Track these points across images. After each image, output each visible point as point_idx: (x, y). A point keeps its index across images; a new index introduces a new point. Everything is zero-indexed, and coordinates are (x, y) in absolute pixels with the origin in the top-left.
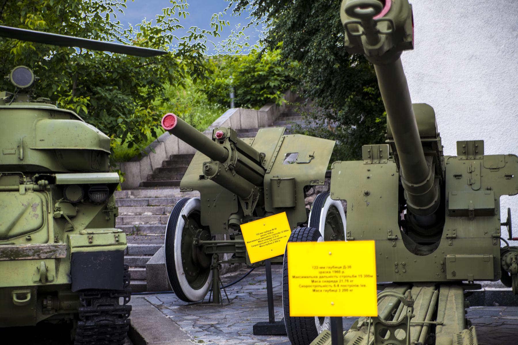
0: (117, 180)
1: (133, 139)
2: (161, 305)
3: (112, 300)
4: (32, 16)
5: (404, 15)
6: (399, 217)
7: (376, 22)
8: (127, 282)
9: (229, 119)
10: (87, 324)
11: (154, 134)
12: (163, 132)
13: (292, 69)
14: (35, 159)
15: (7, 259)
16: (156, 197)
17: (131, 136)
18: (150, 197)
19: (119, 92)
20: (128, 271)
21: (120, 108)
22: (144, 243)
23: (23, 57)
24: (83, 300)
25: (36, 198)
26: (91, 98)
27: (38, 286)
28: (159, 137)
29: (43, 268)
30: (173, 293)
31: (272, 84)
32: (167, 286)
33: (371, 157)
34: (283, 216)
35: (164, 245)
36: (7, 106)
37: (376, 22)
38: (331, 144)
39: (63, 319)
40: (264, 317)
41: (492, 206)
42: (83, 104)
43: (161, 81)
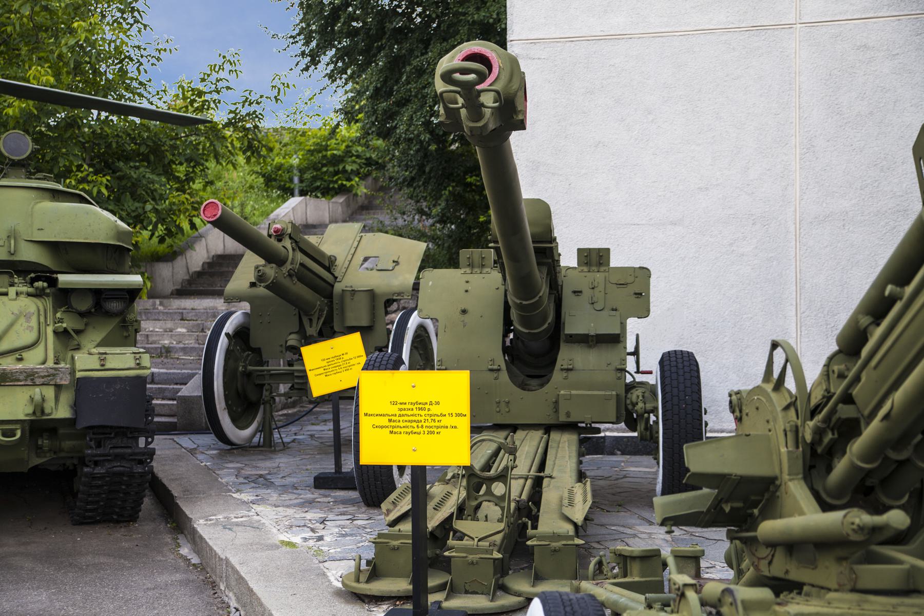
2: (195, 449)
6: (504, 342)
9: (291, 209)
11: (193, 226)
13: (376, 149)
14: (30, 254)
22: (175, 368)
24: (91, 440)
25: (31, 305)
27: (31, 421)
29: (38, 397)
31: (349, 168)
33: (471, 265)
35: (201, 372)
38: (421, 247)
39: (64, 464)
40: (328, 466)
41: (617, 331)
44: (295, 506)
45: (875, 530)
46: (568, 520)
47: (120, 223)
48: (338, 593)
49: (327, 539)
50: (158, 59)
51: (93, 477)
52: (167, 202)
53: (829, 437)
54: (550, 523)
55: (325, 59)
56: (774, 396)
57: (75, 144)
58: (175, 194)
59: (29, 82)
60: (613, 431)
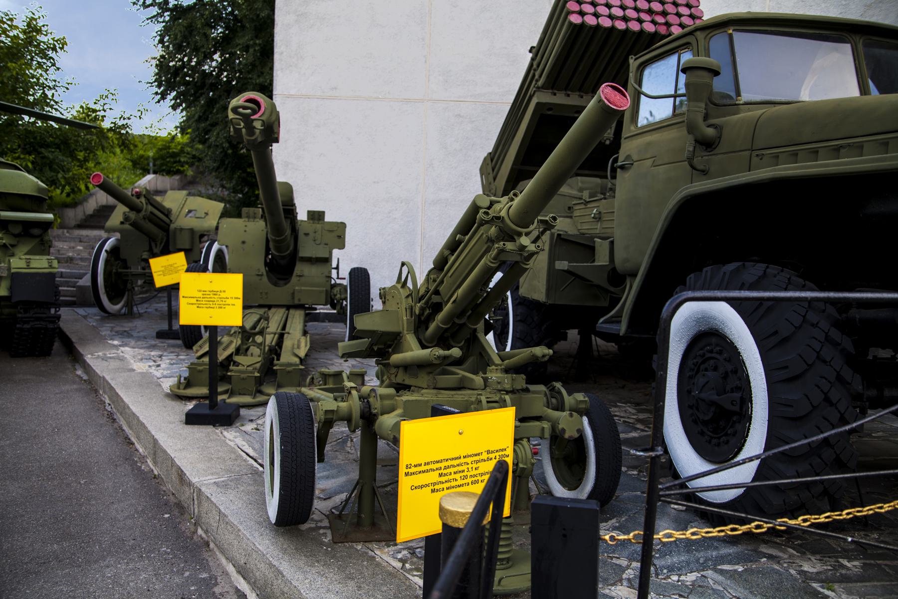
5: (273, 118)
6: (265, 260)
7: (253, 120)
9: (147, 180)
11: (87, 188)
13: (197, 149)
31: (182, 160)
33: (248, 217)
34: (182, 255)
37: (253, 120)
38: (221, 206)
40: (165, 326)
41: (327, 256)
44: (144, 348)
45: (445, 358)
46: (297, 356)
48: (168, 396)
49: (163, 366)
50: (67, 89)
53: (427, 312)
54: (286, 357)
55: (170, 97)
56: (401, 290)
58: (76, 168)
60: (324, 309)
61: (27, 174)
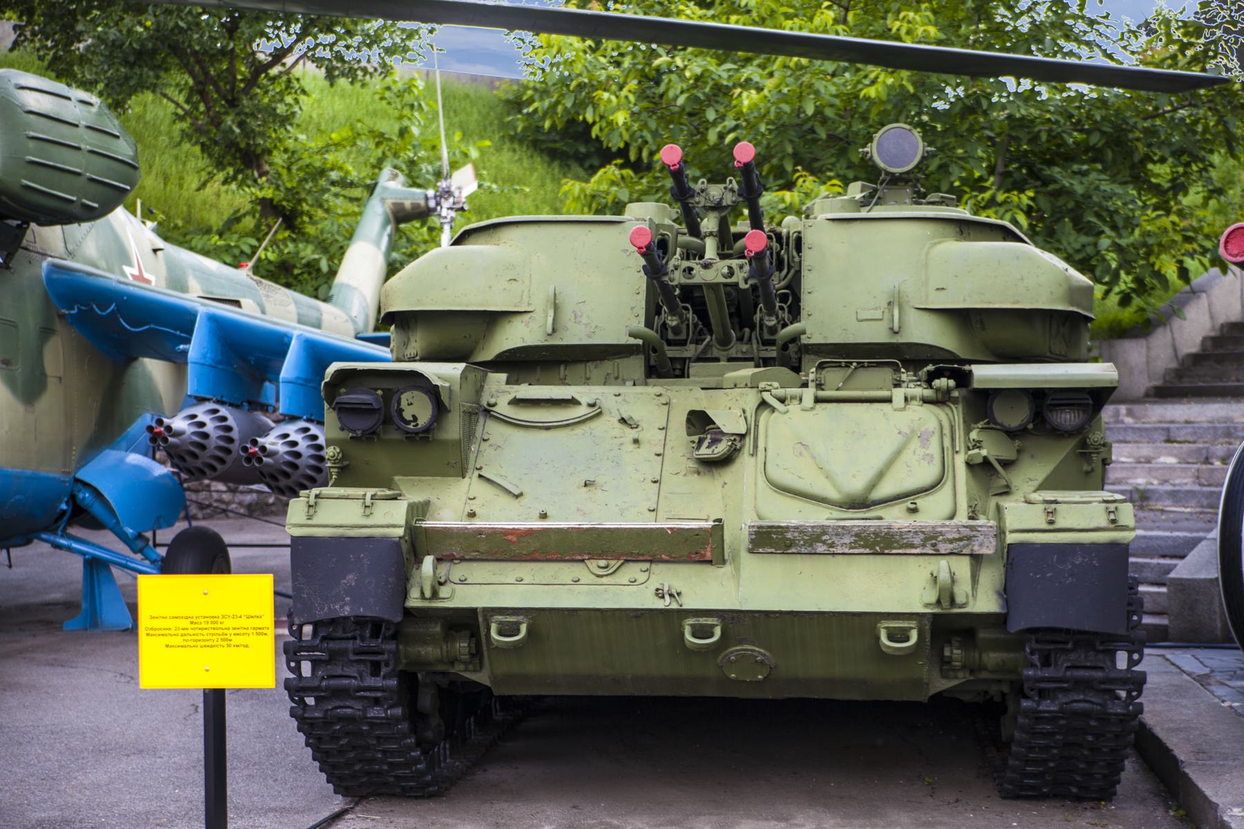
0: (1111, 381)
1: (1132, 285)
2: (1207, 676)
3: (1101, 657)
4: (911, 14)
8: (1135, 618)
10: (1041, 708)
11: (1184, 273)
12: (1206, 269)
14: (925, 332)
15: (867, 551)
16: (1187, 422)
17: (1129, 279)
18: (1172, 422)
19: (1103, 177)
20: (1137, 592)
21: (1105, 214)
22: (1159, 528)
23: (889, 107)
24: (1032, 653)
25: (929, 418)
26: (1036, 193)
27: (934, 615)
28: (1196, 280)
29: (944, 576)
30: (1237, 648)
32: (1219, 632)
35: (1216, 533)
36: (864, 213)
39: (986, 692)
42: (1019, 207)
43: (1204, 149)
44: (103, 751)
47: (1073, 273)
51: (1037, 717)
52: (1137, 232)
57: (979, 139)
59: (899, 39)
61: (1038, 251)
